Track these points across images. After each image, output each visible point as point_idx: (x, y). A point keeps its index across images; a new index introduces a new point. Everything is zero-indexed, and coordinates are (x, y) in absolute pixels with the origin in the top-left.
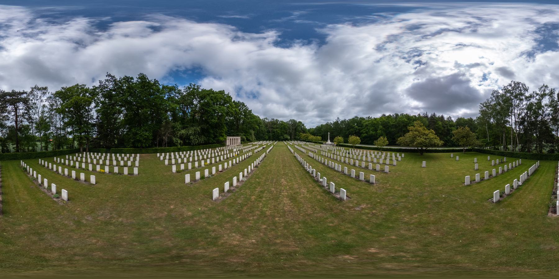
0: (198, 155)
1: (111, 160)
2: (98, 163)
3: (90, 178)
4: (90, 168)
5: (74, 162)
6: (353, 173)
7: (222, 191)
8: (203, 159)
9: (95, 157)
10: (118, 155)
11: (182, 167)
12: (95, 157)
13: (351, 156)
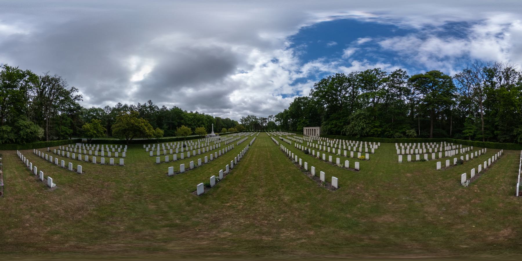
0: (342, 145)
1: (363, 148)
2: (352, 150)
3: (336, 160)
4: (345, 153)
5: (331, 148)
6: (63, 163)
7: (469, 176)
8: (347, 149)
9: (350, 145)
10: (370, 143)
11: (433, 156)
12: (350, 145)
13: (85, 152)
